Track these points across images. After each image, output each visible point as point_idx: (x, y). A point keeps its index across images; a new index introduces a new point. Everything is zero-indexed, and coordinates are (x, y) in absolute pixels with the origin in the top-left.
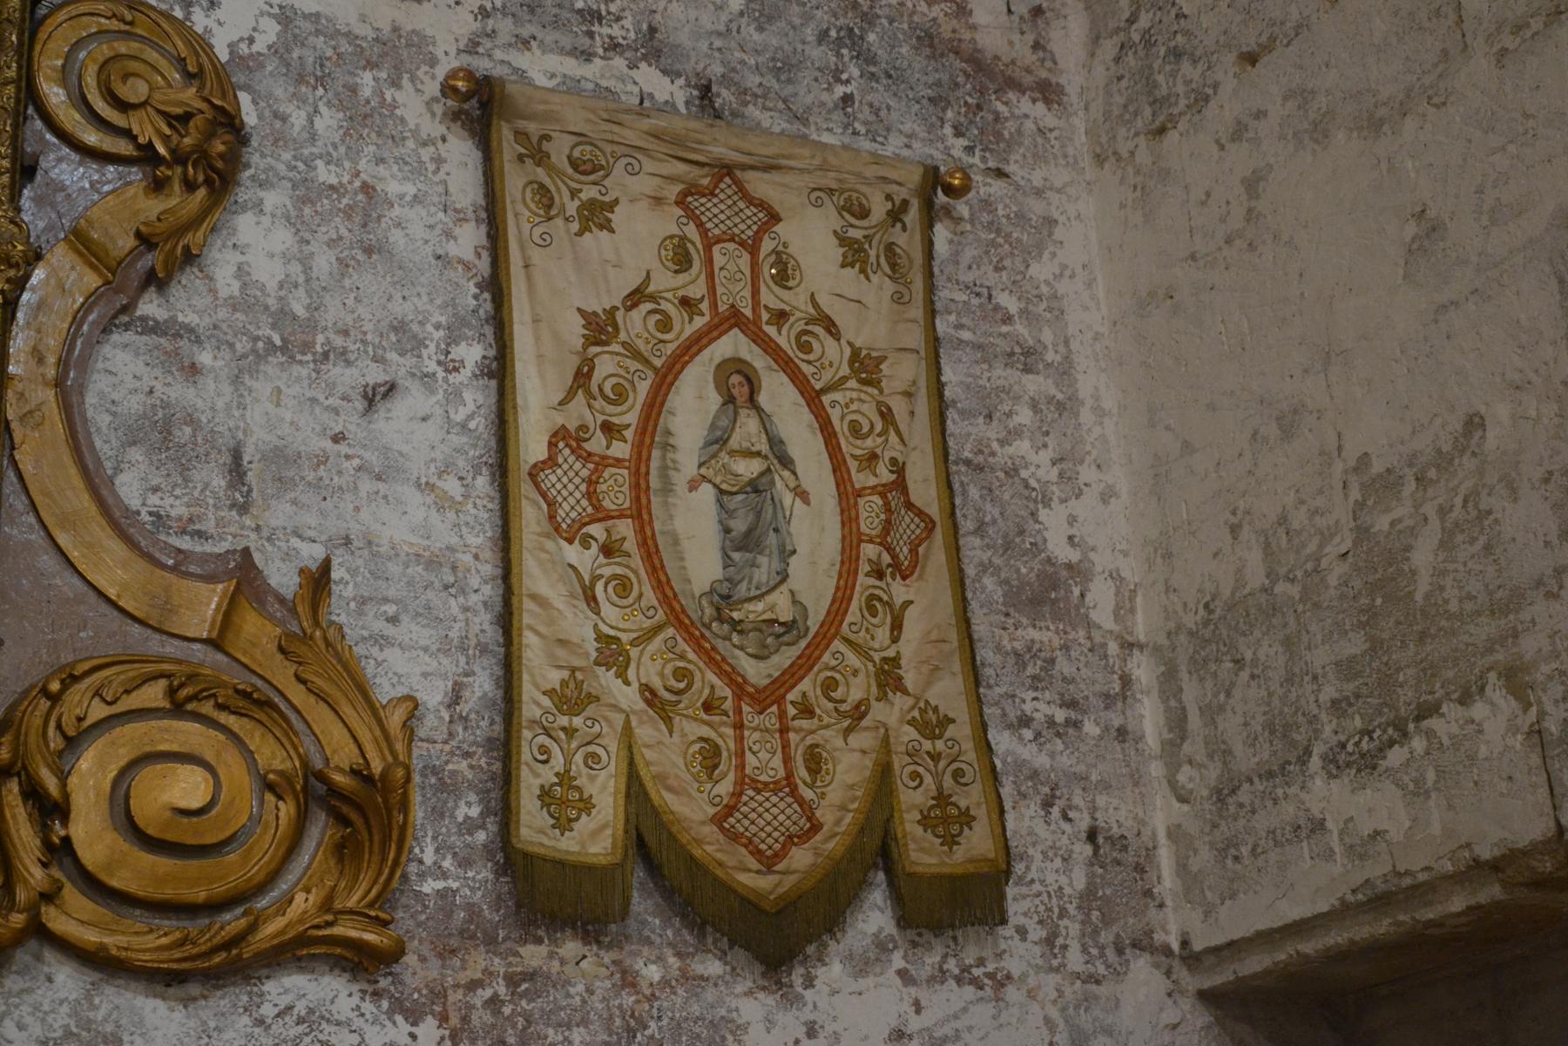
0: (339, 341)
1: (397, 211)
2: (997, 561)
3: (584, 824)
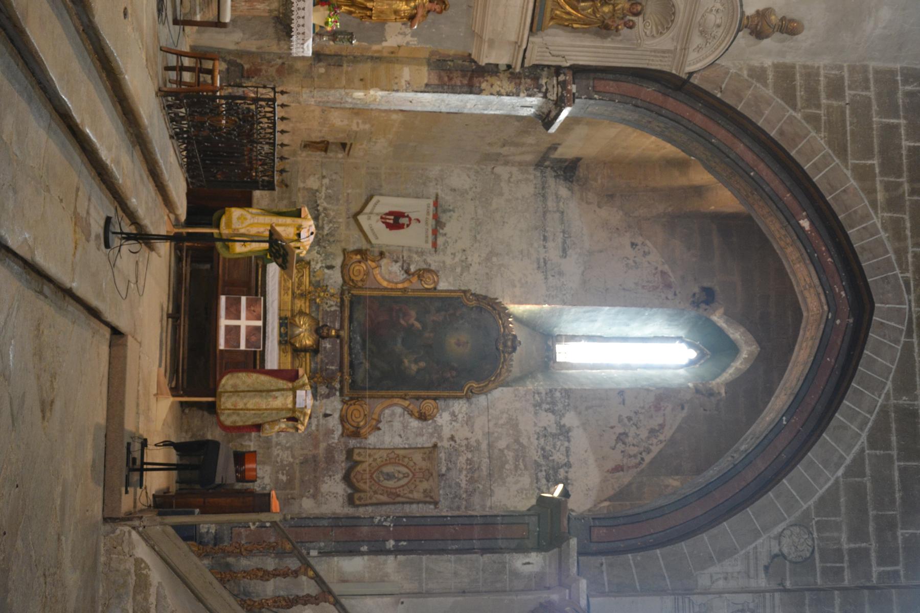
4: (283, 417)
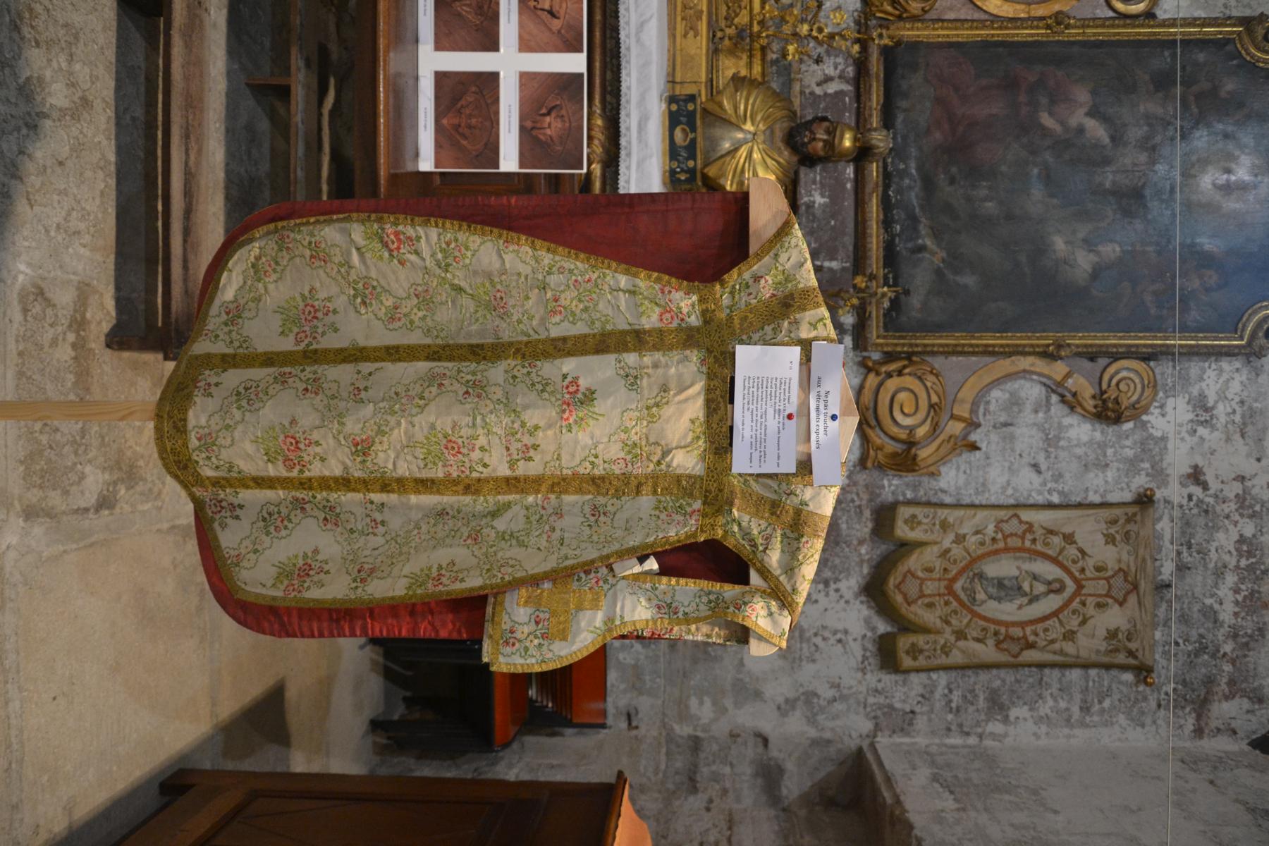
0: (1053, 456)
1: (1101, 475)
2: (1007, 687)
3: (906, 528)
4: (635, 540)
